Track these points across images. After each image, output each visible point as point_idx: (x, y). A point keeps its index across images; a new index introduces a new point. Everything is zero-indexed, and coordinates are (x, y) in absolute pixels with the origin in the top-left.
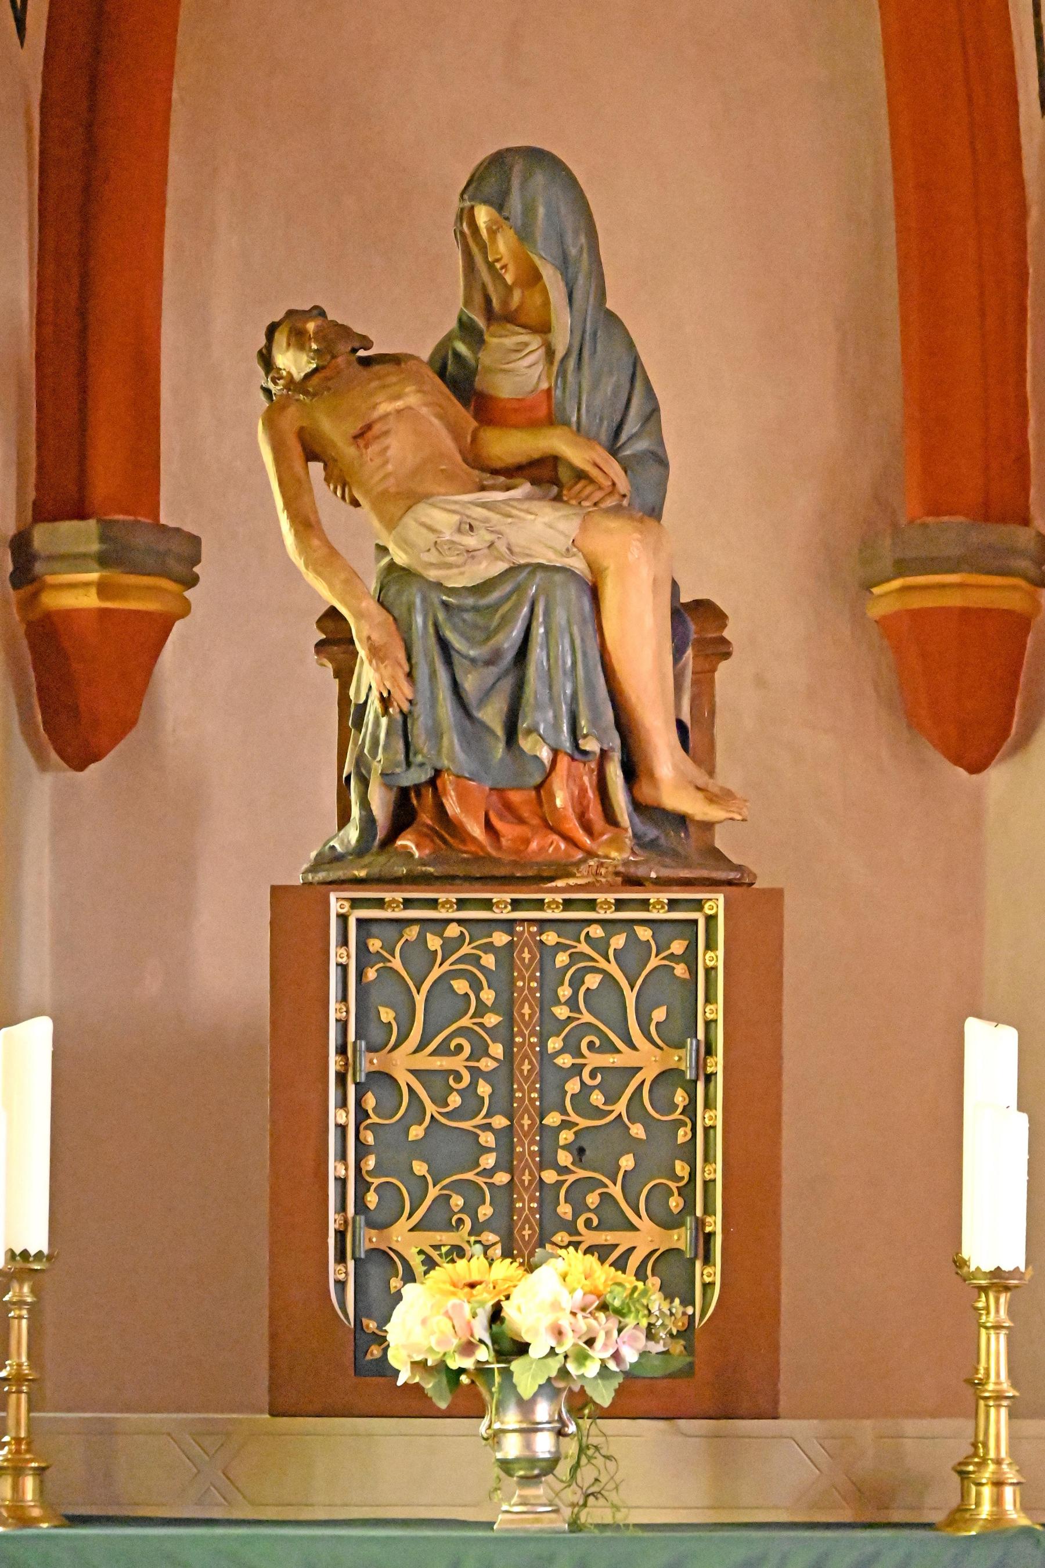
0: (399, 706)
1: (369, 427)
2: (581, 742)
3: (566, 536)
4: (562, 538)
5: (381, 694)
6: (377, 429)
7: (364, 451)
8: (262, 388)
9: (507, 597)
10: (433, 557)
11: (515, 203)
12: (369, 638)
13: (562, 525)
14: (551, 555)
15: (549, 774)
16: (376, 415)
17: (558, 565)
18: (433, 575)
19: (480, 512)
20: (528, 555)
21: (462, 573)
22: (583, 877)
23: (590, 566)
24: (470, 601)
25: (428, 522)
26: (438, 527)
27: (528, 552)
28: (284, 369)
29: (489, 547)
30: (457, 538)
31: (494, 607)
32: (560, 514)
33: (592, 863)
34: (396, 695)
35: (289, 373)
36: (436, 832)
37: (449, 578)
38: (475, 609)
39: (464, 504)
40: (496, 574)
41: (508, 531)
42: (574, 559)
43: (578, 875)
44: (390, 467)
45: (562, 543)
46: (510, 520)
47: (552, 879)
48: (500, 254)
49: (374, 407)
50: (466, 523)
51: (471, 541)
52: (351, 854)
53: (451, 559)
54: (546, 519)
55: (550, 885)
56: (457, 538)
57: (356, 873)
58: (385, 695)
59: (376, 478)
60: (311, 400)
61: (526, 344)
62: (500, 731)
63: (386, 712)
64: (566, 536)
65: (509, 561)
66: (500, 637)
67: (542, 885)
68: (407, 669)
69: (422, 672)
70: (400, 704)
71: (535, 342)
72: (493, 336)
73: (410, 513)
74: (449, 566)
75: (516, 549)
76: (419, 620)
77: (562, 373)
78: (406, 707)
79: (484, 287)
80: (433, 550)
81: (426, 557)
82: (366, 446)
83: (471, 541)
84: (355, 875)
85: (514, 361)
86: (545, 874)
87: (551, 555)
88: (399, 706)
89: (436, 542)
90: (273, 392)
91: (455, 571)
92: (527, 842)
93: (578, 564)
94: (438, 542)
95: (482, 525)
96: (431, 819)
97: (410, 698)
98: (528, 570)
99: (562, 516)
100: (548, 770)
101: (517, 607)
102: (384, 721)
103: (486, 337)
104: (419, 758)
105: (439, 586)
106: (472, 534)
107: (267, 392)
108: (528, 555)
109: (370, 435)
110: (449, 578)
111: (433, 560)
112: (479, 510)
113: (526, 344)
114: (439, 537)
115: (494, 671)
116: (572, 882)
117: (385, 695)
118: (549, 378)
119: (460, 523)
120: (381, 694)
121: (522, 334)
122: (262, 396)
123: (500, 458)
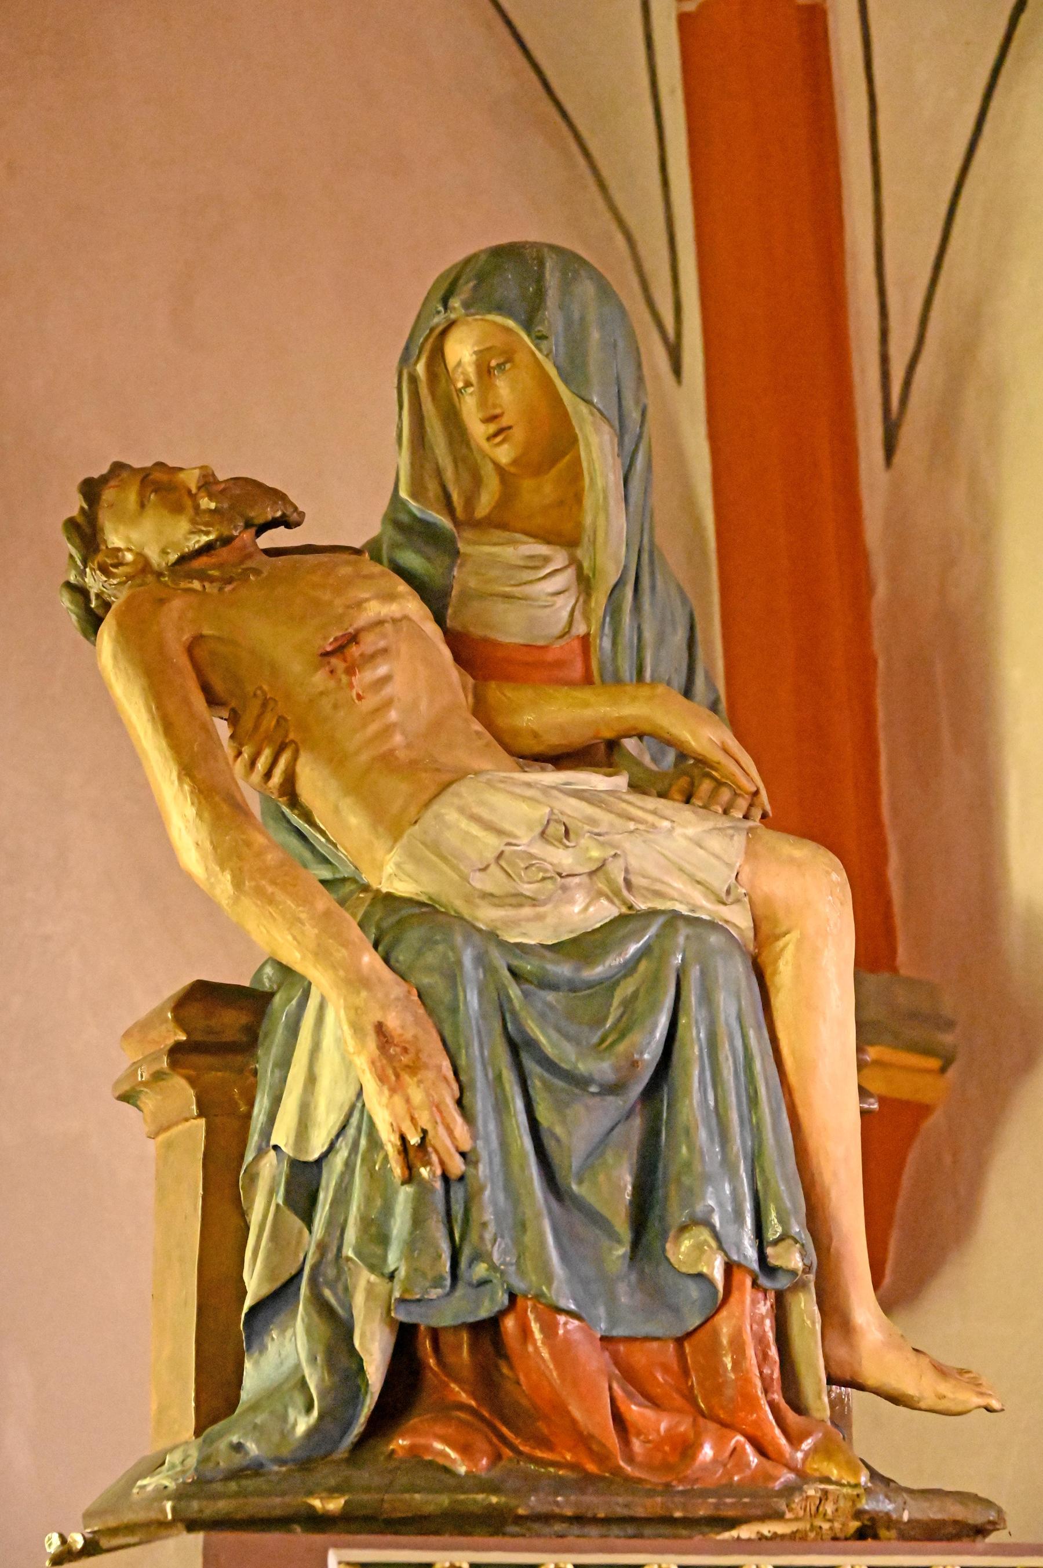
0: (442, 1163)
1: (354, 638)
2: (769, 1251)
3: (729, 866)
4: (725, 870)
5: (403, 1139)
6: (370, 643)
7: (344, 679)
8: (68, 585)
9: (630, 968)
10: (491, 882)
11: (552, 315)
12: (380, 1028)
13: (715, 843)
14: (698, 897)
15: (718, 1310)
16: (363, 619)
17: (705, 917)
18: (486, 915)
19: (574, 808)
20: (659, 894)
21: (540, 918)
22: (797, 1519)
23: (756, 928)
24: (563, 970)
25: (484, 813)
26: (507, 826)
27: (658, 887)
28: (129, 550)
29: (592, 874)
30: (538, 849)
31: (610, 984)
32: (710, 824)
33: (811, 1492)
34: (440, 1138)
35: (140, 556)
36: (483, 1419)
37: (515, 923)
38: (573, 987)
39: (546, 790)
40: (598, 925)
41: (627, 845)
42: (735, 907)
43: (788, 1515)
44: (393, 715)
45: (721, 879)
46: (632, 826)
47: (732, 1523)
48: (501, 406)
49: (359, 604)
50: (558, 821)
51: (563, 858)
52: (282, 1462)
53: (527, 889)
54: (690, 831)
55: (726, 1535)
56: (538, 849)
57: (317, 1503)
58: (414, 1140)
59: (359, 738)
60: (221, 589)
61: (546, 560)
62: (623, 1229)
63: (411, 1177)
64: (729, 866)
65: (624, 902)
66: (635, 1037)
67: (712, 1536)
68: (457, 1094)
69: (481, 1102)
70: (446, 1159)
71: (560, 558)
72: (469, 542)
73: (446, 797)
74: (518, 900)
75: (636, 880)
76: (473, 999)
77: (614, 609)
78: (457, 1166)
79: (439, 473)
80: (494, 869)
81: (480, 882)
82: (350, 671)
83: (563, 858)
84: (312, 1507)
85: (531, 582)
86: (730, 1513)
87: (698, 897)
88: (442, 1163)
89: (502, 853)
90: (93, 592)
91: (527, 911)
92: (688, 1449)
93: (739, 919)
94: (507, 854)
95: (587, 828)
96: (473, 1395)
97: (466, 1147)
98: (661, 920)
99: (715, 829)
100: (719, 1302)
101: (655, 981)
102: (404, 1195)
103: (461, 546)
104: (481, 1270)
105: (492, 936)
106: (568, 843)
107: (80, 592)
108: (659, 894)
109: (354, 651)
110: (515, 923)
111: (489, 888)
112: (573, 802)
113: (546, 560)
114: (509, 844)
115: (615, 1105)
116: (767, 1529)
117: (414, 1140)
118: (587, 618)
119: (548, 822)
120: (403, 1139)
121: (530, 543)
122: (66, 601)
123: (536, 735)
